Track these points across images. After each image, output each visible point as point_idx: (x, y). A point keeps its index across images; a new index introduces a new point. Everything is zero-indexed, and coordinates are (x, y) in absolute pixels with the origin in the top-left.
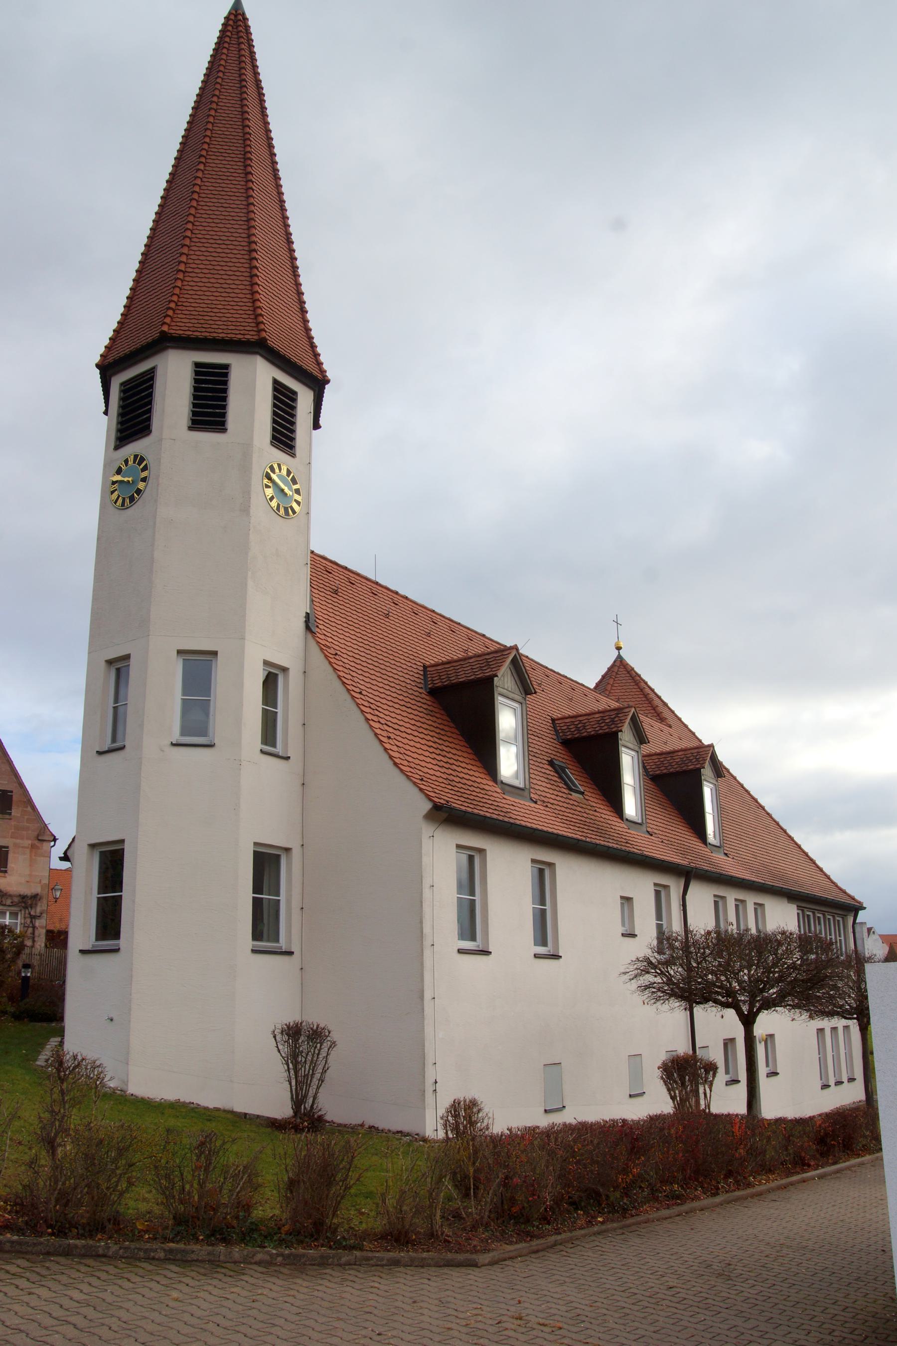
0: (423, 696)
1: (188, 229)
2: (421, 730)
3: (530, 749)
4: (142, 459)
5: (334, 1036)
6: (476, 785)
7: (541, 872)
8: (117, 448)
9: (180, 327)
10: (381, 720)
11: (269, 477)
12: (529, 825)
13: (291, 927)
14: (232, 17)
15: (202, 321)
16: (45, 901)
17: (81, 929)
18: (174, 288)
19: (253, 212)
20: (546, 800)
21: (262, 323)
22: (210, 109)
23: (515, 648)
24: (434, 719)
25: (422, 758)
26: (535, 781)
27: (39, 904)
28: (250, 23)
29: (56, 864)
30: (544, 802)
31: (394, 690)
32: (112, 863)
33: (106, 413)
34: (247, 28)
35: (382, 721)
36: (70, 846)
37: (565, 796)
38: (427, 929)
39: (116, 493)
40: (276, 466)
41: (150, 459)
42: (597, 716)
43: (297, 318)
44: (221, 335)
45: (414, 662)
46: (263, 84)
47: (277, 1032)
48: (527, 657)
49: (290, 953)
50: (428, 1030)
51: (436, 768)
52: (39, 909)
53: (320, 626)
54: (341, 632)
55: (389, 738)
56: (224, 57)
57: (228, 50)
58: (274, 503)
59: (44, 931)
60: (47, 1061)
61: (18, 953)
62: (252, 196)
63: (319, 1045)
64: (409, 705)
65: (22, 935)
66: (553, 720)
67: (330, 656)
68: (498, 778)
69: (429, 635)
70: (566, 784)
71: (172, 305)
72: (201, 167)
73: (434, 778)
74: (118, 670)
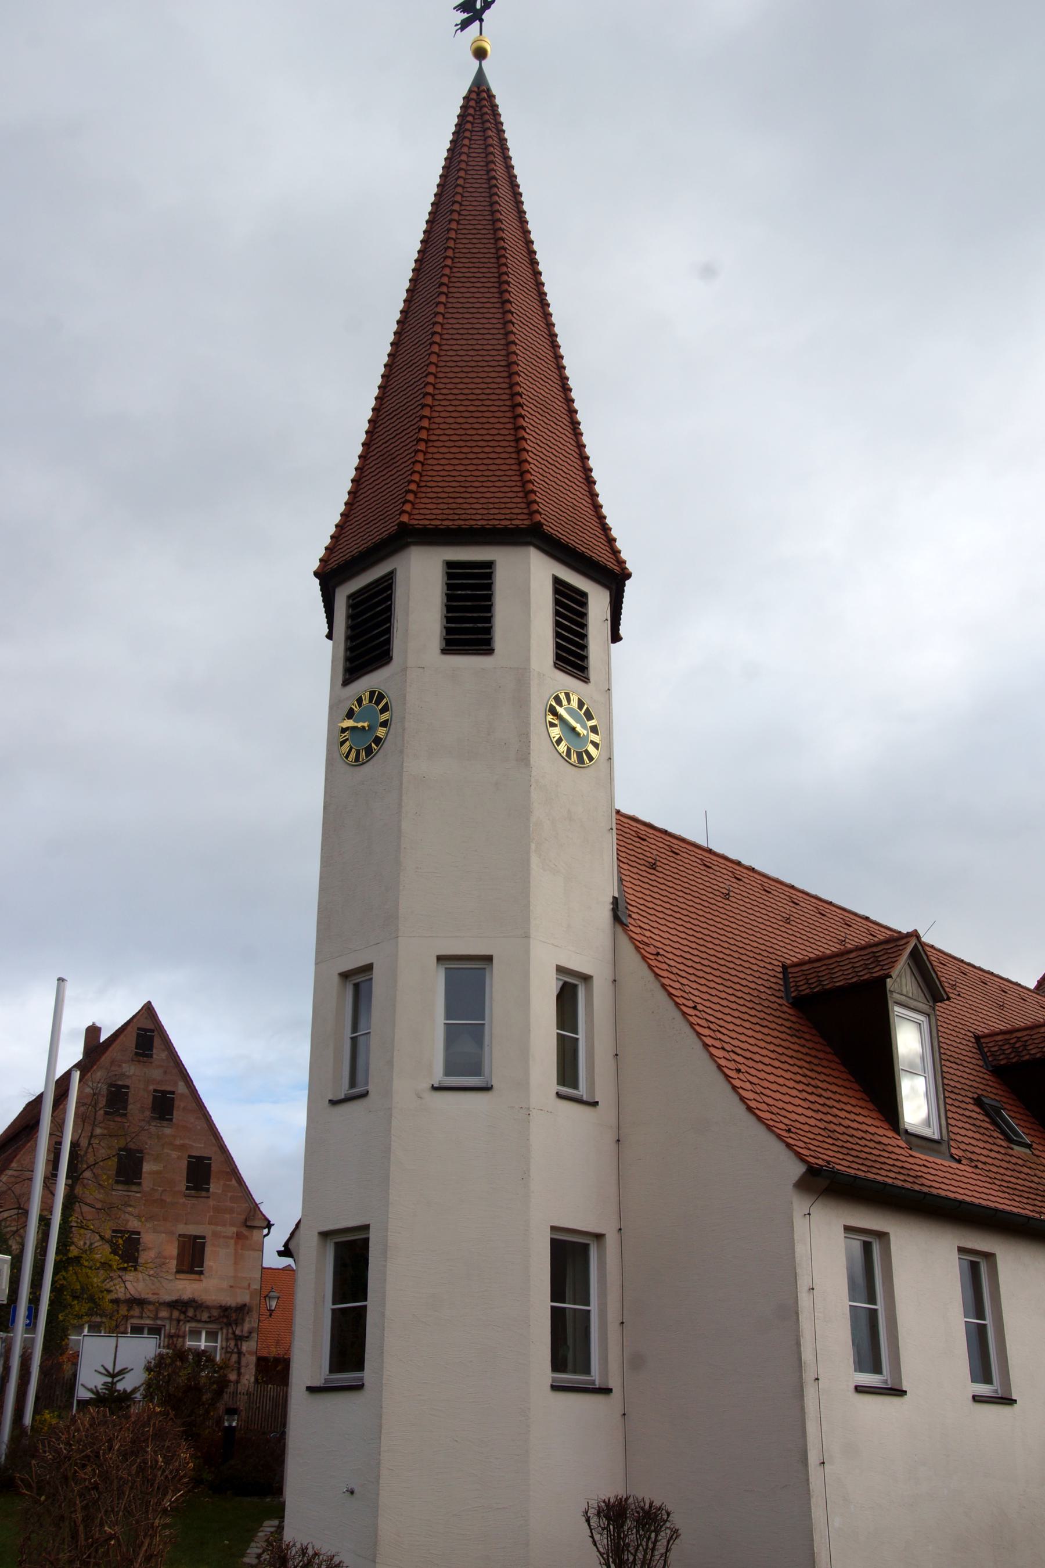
0: (785, 1009)
1: (428, 383)
2: (783, 1058)
3: (946, 1081)
4: (381, 697)
5: (677, 1520)
6: (868, 1136)
7: (974, 1267)
8: (346, 683)
9: (426, 515)
10: (726, 1046)
11: (553, 712)
12: (952, 1195)
13: (606, 1353)
14: (473, 96)
15: (454, 506)
16: (255, 1314)
17: (309, 1357)
18: (414, 463)
19: (515, 353)
20: (974, 1157)
21: (535, 502)
22: (450, 221)
23: (915, 934)
24: (803, 1042)
25: (787, 1098)
26: (956, 1130)
27: (247, 1319)
28: (497, 101)
29: (272, 1259)
30: (971, 1160)
31: (741, 1002)
32: (351, 1258)
33: (329, 636)
34: (494, 107)
35: (727, 1047)
36: (292, 1234)
37: (1002, 1151)
38: (807, 1355)
39: (347, 744)
40: (562, 696)
41: (392, 696)
42: (999, 1038)
43: (581, 492)
44: (480, 523)
45: (768, 960)
46: (519, 181)
47: (592, 1512)
48: (932, 947)
49: (607, 1391)
50: (817, 1513)
51: (809, 1113)
52: (246, 1327)
53: (634, 916)
54: (663, 922)
55: (739, 1071)
56: (465, 150)
57: (470, 140)
58: (562, 748)
59: (254, 1358)
60: (259, 1556)
61: (219, 1393)
62: (512, 332)
63: (653, 1535)
64: (765, 1023)
65: (225, 1366)
66: (978, 1038)
67: (650, 957)
68: (901, 1127)
69: (787, 921)
70: (1003, 1132)
71: (413, 487)
72: (443, 299)
73: (806, 1128)
74: (357, 986)
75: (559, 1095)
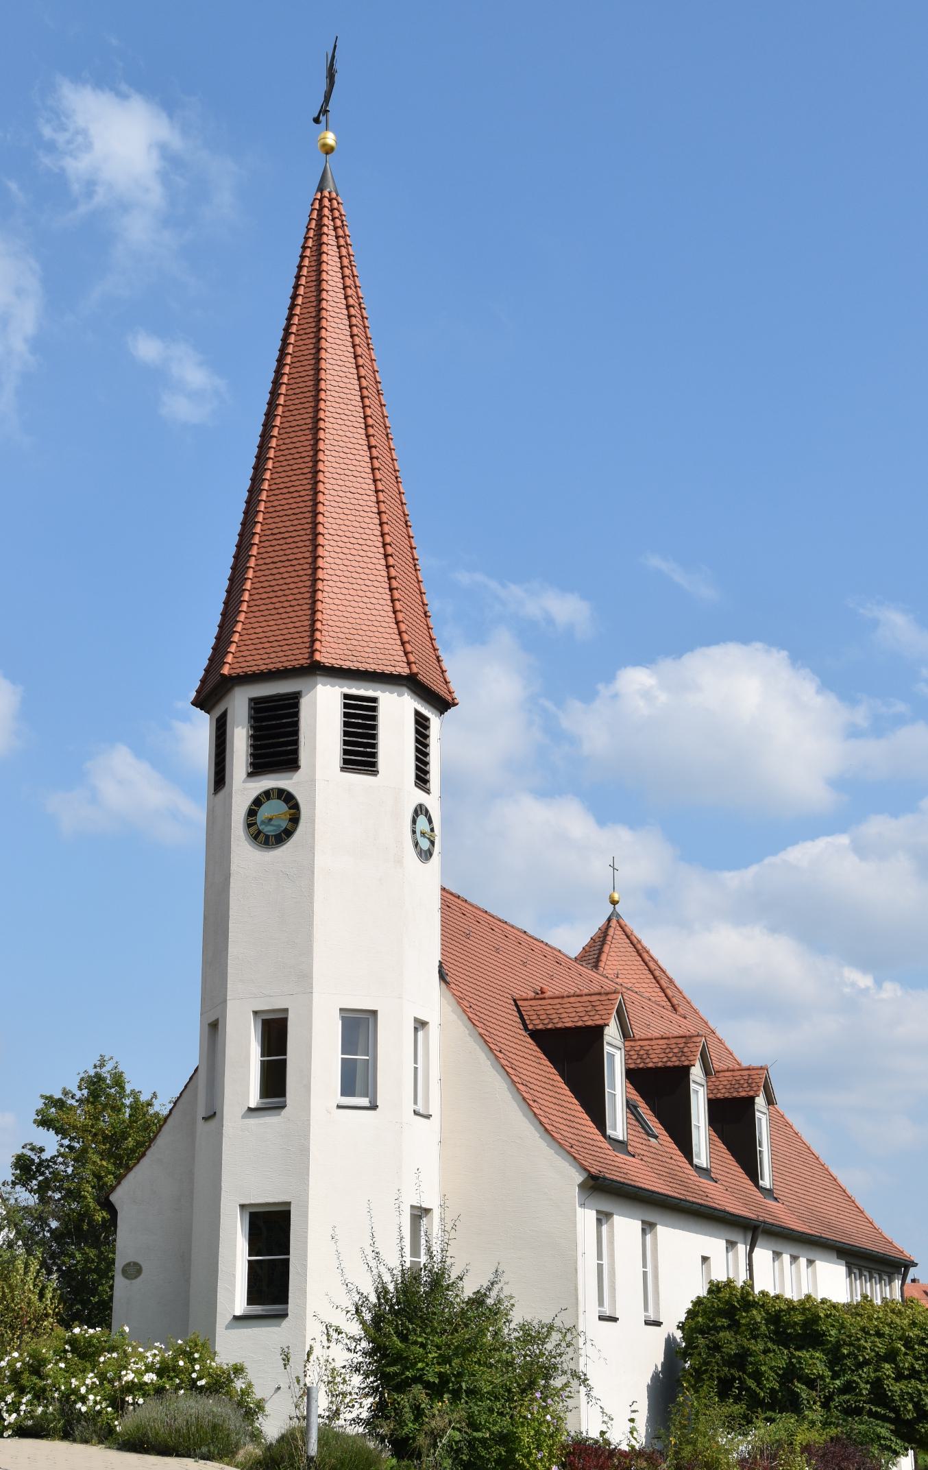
70: (643, 1128)
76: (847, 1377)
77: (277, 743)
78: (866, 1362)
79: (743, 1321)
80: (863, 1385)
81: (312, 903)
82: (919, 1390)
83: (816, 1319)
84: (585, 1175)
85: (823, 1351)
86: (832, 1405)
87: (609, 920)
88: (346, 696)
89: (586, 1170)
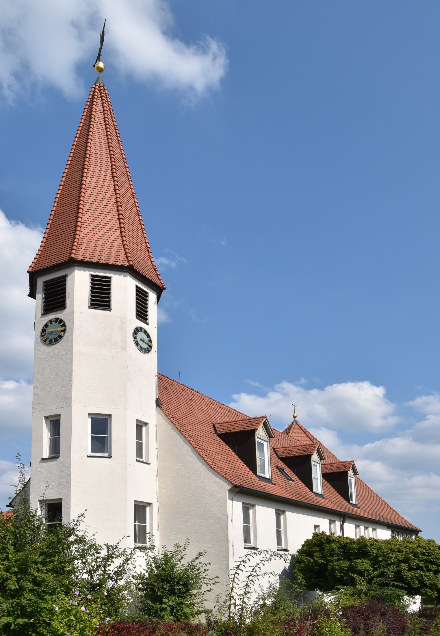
38: (230, 538)
70: (285, 477)
75: (137, 461)
76: (382, 570)
77: (55, 298)
78: (392, 564)
79: (326, 548)
80: (390, 573)
81: (72, 366)
82: (421, 575)
83: (365, 546)
84: (232, 486)
85: (369, 559)
86: (373, 582)
87: (293, 423)
88: (92, 276)
89: (232, 483)
